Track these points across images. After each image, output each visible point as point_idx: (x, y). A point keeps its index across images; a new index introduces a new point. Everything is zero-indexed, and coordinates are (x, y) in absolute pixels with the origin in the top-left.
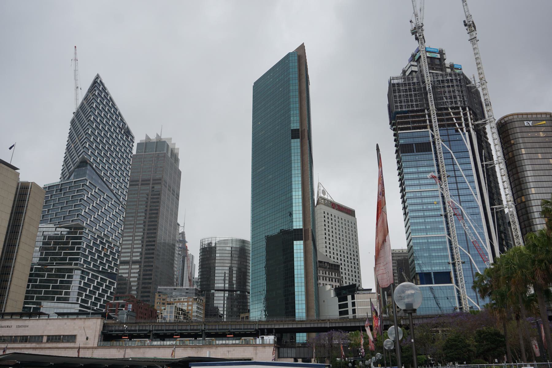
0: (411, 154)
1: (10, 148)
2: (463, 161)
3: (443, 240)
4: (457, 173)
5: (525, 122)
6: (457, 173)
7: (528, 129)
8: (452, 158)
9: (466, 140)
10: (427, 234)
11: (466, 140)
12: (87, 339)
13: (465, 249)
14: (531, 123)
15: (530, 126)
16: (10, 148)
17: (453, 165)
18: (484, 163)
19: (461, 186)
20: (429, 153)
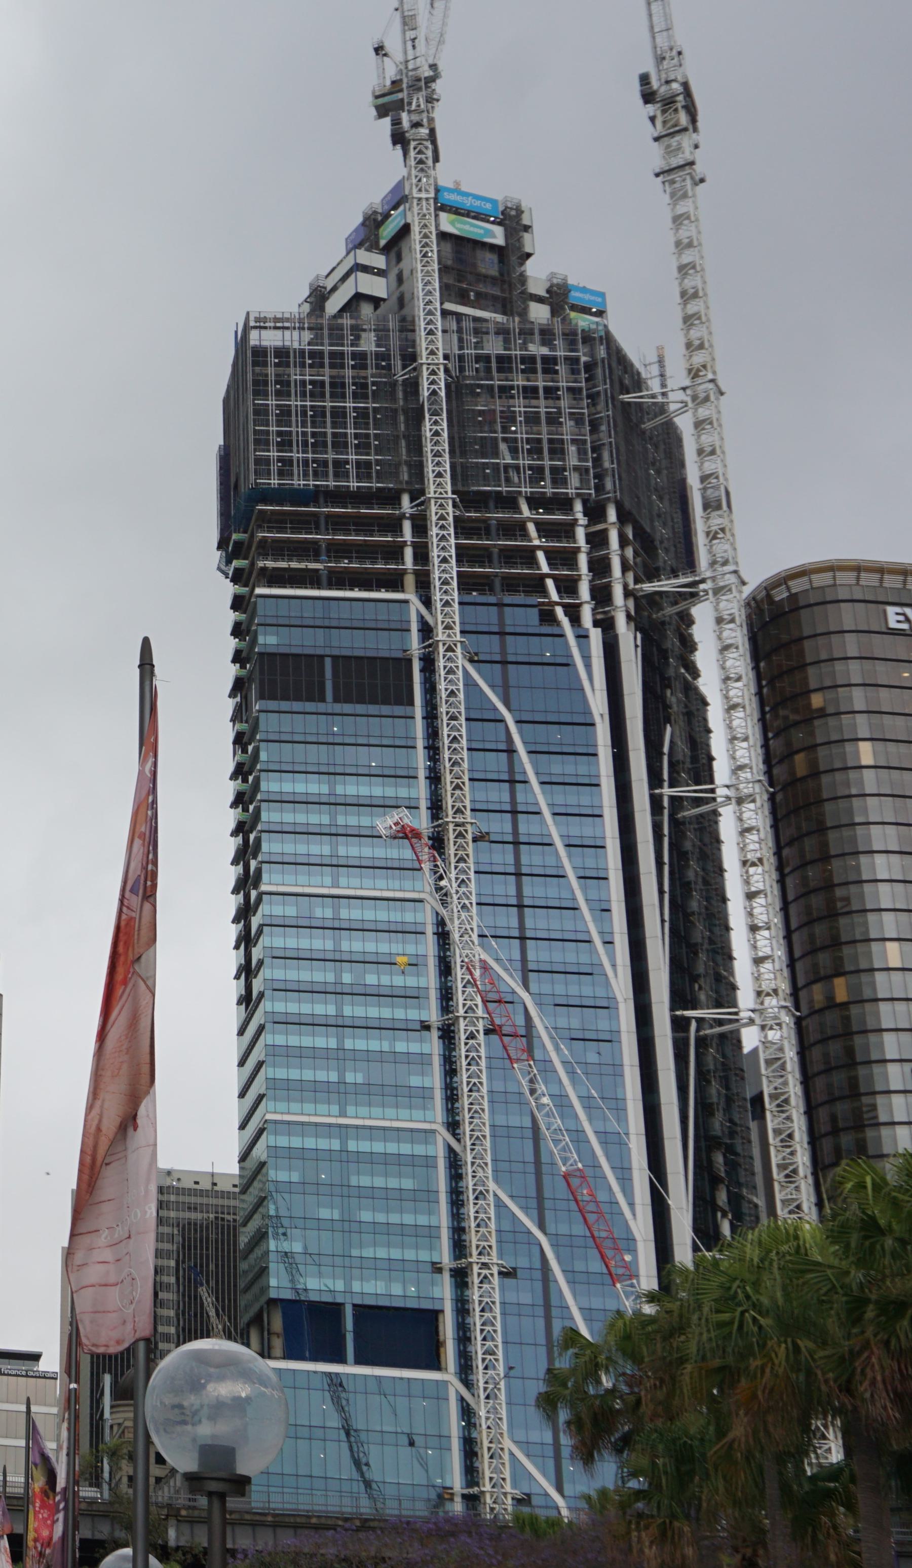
0: (310, 706)
2: (558, 767)
3: (419, 1150)
6: (526, 826)
8: (511, 751)
9: (588, 666)
10: (343, 1114)
11: (588, 666)
17: (512, 782)
20: (399, 710)
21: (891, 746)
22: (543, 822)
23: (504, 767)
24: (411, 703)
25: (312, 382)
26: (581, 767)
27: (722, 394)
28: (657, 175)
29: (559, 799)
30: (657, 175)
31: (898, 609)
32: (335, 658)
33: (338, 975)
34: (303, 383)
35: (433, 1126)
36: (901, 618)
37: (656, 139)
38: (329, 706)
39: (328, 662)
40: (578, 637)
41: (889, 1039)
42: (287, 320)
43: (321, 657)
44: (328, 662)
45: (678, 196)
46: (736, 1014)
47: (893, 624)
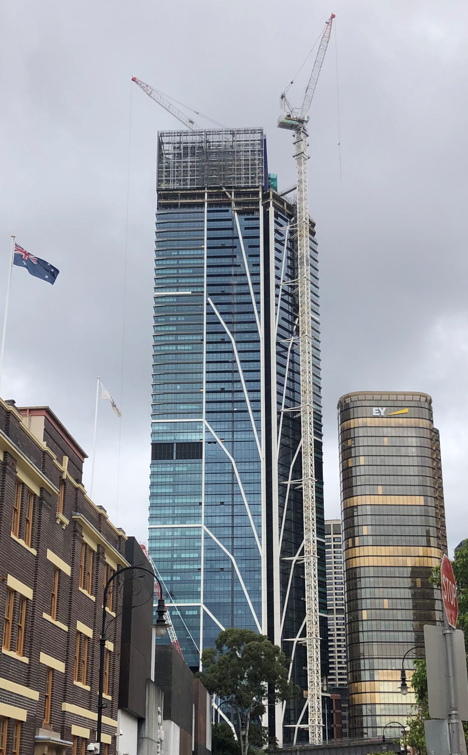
0: (168, 461)
1: (47, 272)
2: (248, 477)
3: (196, 533)
4: (236, 499)
5: (374, 409)
6: (236, 499)
7: (377, 422)
8: (233, 473)
9: (260, 441)
10: (173, 524)
11: (260, 441)
12: (292, 83)
13: (228, 549)
14: (383, 411)
15: (382, 417)
16: (47, 272)
17: (233, 484)
18: (289, 482)
19: (239, 437)
20: (197, 460)
21: (370, 458)
22: (242, 496)
23: (231, 478)
24: (201, 458)
25: (177, 153)
26: (253, 337)
27: (307, 136)
28: (294, 157)
29: (248, 489)
30: (294, 157)
31: (377, 408)
32: (177, 443)
33: (173, 543)
34: (174, 171)
35: (201, 525)
36: (377, 411)
37: (294, 144)
38: (175, 461)
39: (175, 444)
40: (257, 431)
41: (364, 612)
42: (172, 133)
43: (173, 443)
44: (175, 444)
45: (300, 164)
46: (301, 481)
47: (374, 414)
